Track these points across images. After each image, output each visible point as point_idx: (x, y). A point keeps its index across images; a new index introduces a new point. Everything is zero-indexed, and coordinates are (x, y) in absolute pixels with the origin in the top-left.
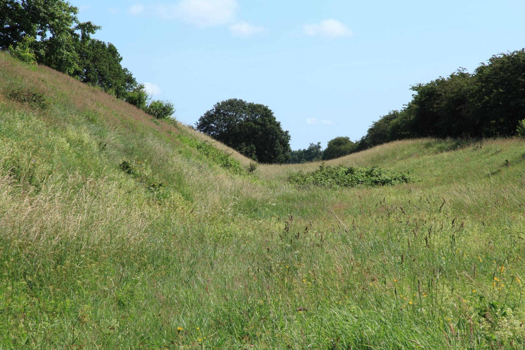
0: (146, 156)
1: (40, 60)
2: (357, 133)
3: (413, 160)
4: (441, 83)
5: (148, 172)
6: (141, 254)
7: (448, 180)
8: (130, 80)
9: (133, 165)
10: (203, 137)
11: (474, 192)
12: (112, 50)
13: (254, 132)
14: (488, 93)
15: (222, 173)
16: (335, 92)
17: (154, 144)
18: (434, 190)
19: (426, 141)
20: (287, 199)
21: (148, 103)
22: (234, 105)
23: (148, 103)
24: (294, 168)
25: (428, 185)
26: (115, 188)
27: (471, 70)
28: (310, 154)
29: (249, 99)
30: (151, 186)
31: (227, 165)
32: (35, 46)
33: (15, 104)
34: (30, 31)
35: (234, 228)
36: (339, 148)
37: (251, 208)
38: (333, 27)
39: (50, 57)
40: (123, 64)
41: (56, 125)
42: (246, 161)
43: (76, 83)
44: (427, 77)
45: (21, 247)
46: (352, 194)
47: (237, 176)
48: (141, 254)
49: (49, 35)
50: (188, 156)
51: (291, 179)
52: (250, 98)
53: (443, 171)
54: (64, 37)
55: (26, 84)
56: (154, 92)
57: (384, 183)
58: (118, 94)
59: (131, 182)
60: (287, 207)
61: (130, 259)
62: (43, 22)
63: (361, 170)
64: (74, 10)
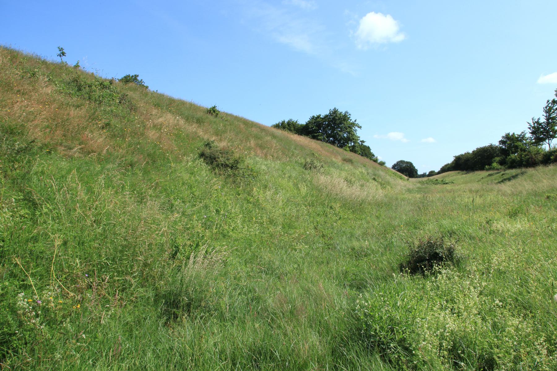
0: (379, 176)
1: (350, 151)
2: (437, 170)
3: (455, 177)
4: (462, 155)
5: (380, 181)
6: (382, 203)
7: (466, 183)
8: (373, 155)
9: (376, 178)
10: (394, 171)
11: (476, 186)
12: (369, 148)
13: (408, 169)
14: (476, 158)
15: (400, 181)
16: (431, 158)
17: (381, 173)
18: (462, 185)
19: (458, 172)
20: (419, 188)
21: (379, 161)
22: (402, 162)
23: (379, 161)
24: (420, 179)
25: (460, 184)
26: (373, 185)
27: (471, 152)
28: (424, 175)
29: (406, 160)
30: (381, 184)
31: (401, 179)
32: (349, 147)
33: (345, 162)
34: (348, 143)
35: (406, 196)
36: (432, 174)
37: (409, 191)
38: (431, 140)
39: (353, 150)
40: (371, 151)
41: (356, 168)
42: (406, 178)
43: (360, 156)
44: (458, 154)
45: (351, 201)
46: (438, 186)
47: (403, 183)
48: (382, 203)
49: (353, 144)
50: (390, 176)
51: (420, 182)
52: (406, 160)
53: (370, 204)
54: (357, 144)
55: (348, 157)
56: (380, 159)
57: (446, 183)
58: (371, 159)
59: (376, 183)
60: (419, 190)
61: (379, 205)
62: (351, 141)
63: (440, 180)
64: (359, 137)
